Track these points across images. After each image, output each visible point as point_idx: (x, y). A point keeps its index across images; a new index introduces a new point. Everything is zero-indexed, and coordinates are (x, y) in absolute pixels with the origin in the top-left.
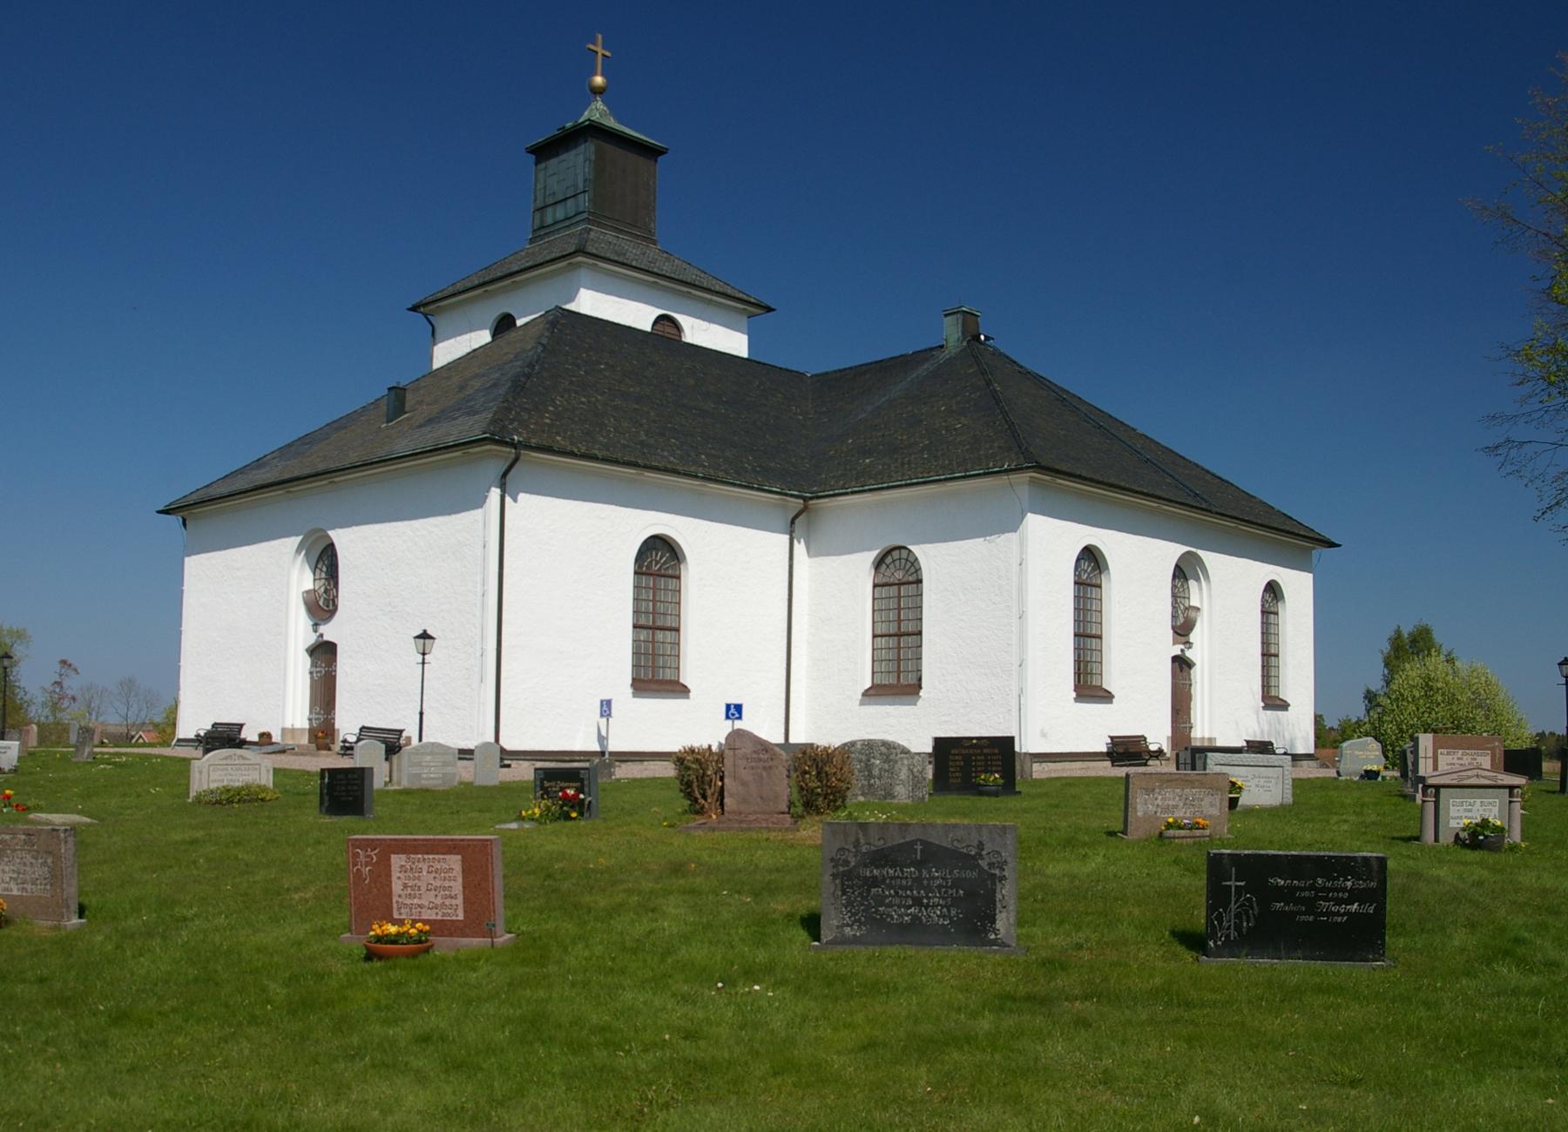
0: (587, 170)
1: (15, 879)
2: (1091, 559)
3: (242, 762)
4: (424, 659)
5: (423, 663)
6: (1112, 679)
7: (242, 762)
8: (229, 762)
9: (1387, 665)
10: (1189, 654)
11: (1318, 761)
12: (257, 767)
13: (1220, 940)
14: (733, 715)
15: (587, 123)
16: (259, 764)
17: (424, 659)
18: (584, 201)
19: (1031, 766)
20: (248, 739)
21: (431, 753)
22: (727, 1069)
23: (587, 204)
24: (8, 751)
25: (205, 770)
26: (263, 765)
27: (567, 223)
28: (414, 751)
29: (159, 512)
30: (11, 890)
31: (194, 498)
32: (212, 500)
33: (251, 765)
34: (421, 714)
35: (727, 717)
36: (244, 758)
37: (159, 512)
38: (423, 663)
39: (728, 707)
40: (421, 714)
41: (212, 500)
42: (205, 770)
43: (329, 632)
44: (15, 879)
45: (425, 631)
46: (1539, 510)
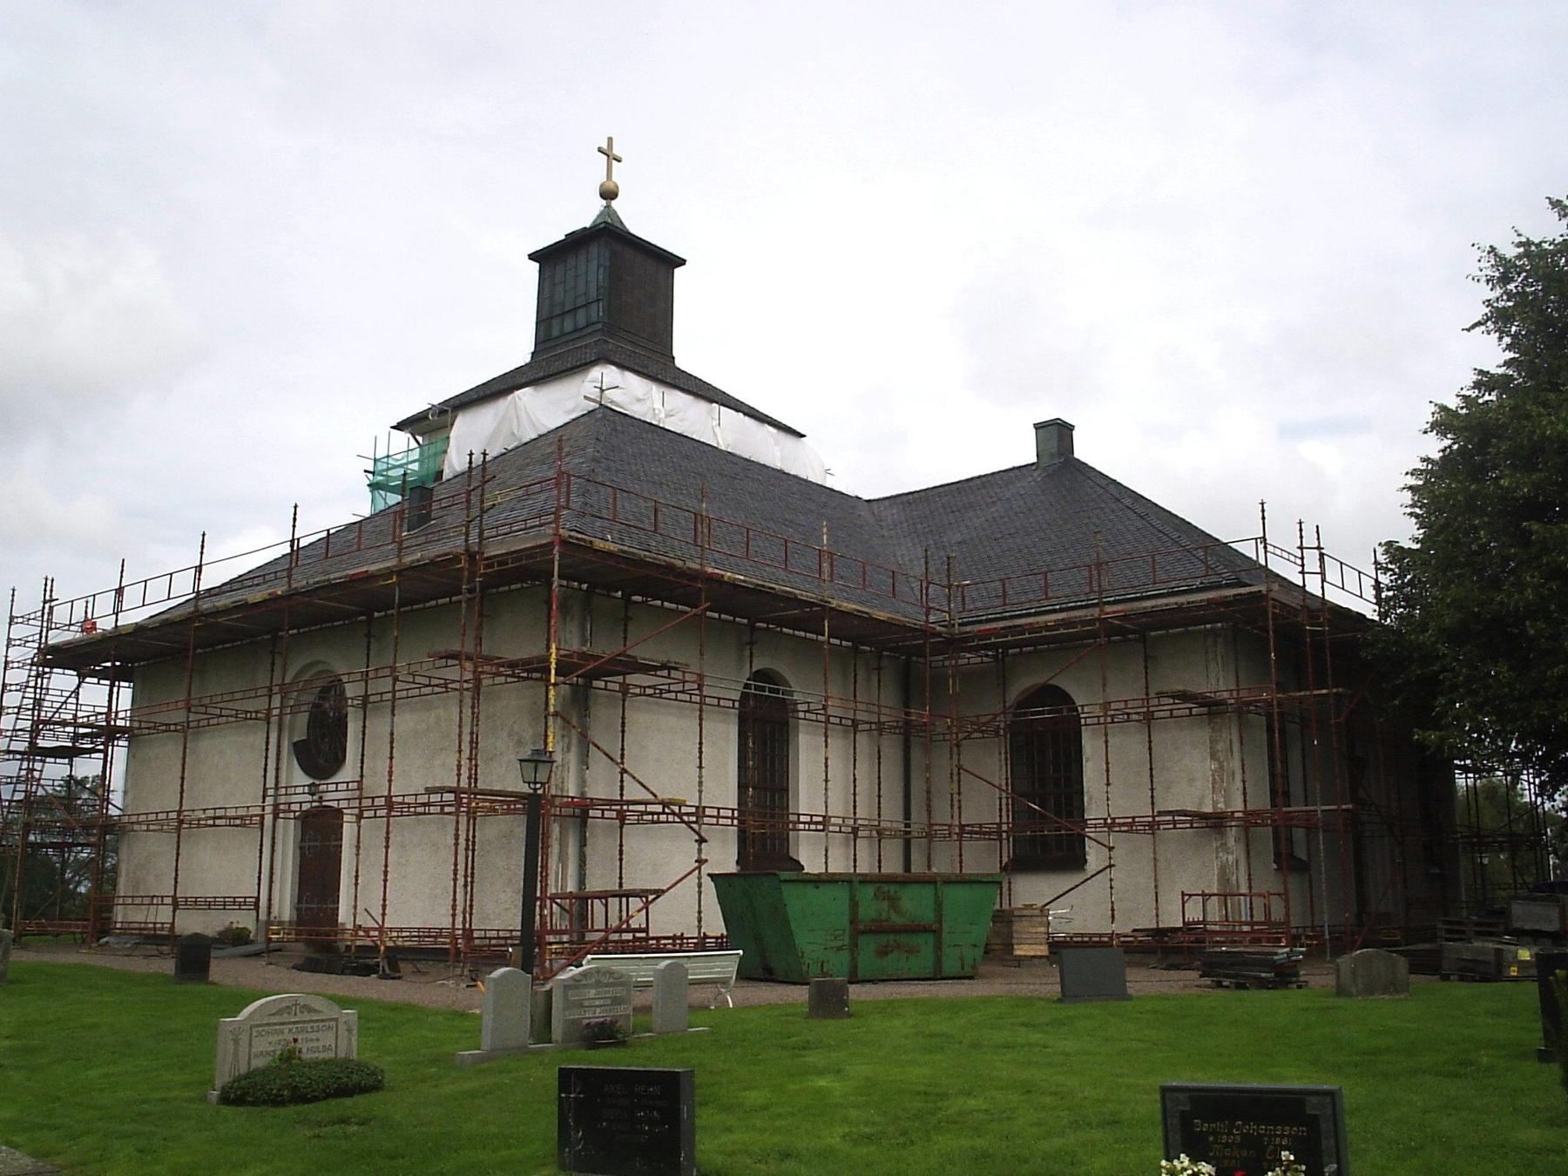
0: (601, 277)
3: (307, 1017)
7: (307, 1017)
8: (285, 1018)
9: (1558, 201)
10: (604, 203)
11: (223, 1075)
12: (333, 1023)
13: (1253, 628)
15: (602, 226)
16: (336, 1020)
18: (598, 311)
19: (1287, 915)
21: (598, 984)
23: (601, 314)
25: (244, 1037)
26: (341, 1020)
27: (577, 335)
28: (571, 982)
32: (980, 882)
33: (323, 1021)
36: (310, 1010)
41: (980, 882)
42: (244, 1037)
46: (1562, 236)
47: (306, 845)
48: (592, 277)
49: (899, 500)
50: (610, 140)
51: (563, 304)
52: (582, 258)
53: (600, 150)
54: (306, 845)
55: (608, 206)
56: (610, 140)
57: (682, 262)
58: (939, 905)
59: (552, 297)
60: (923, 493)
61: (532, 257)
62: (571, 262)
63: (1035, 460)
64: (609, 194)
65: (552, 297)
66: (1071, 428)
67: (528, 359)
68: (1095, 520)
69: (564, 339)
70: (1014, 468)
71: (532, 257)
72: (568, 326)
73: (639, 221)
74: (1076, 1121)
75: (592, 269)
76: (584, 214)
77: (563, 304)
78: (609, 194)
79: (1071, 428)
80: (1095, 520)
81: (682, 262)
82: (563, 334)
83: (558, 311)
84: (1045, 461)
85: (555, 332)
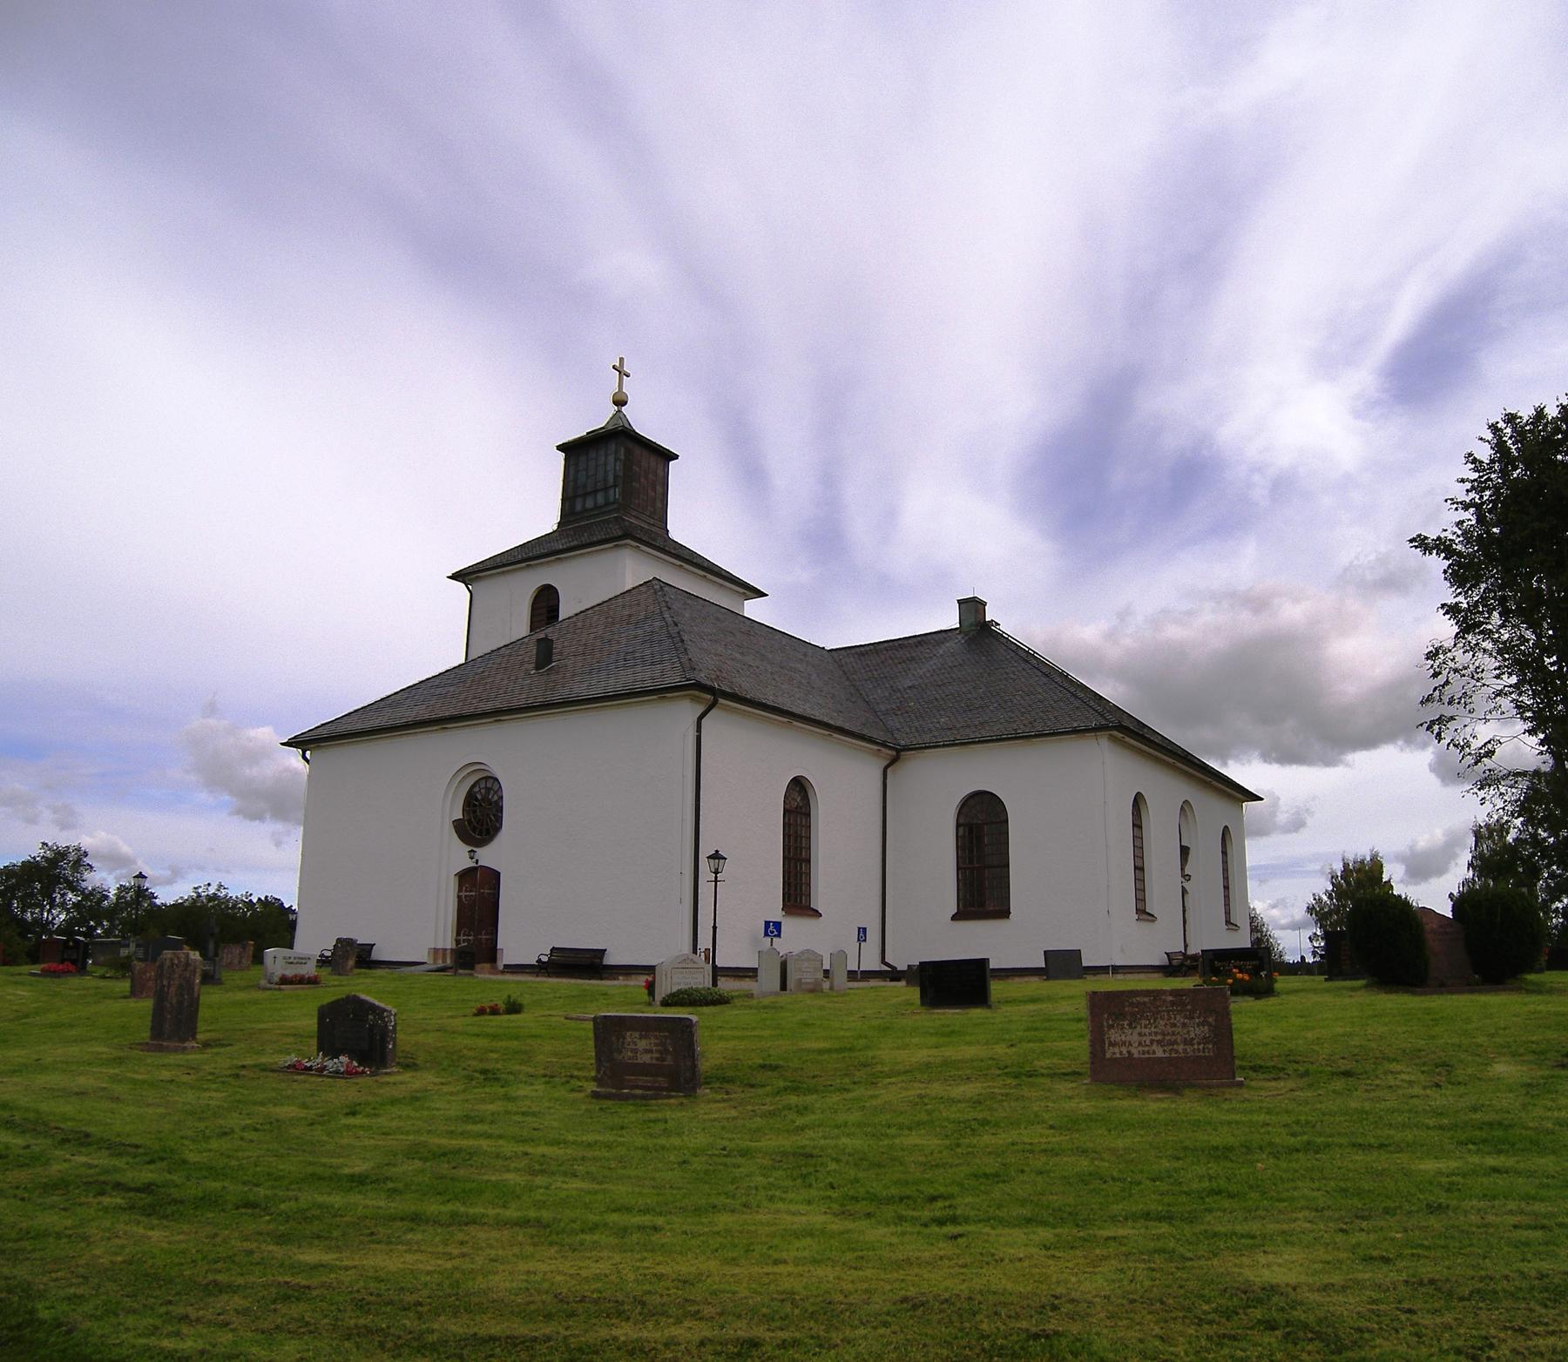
1: (1159, 1042)
2: (799, 788)
4: (716, 877)
5: (716, 881)
6: (818, 902)
14: (772, 932)
17: (716, 877)
20: (1289, 931)
22: (257, 1330)
24: (309, 962)
29: (282, 744)
30: (1154, 1052)
31: (324, 732)
34: (715, 928)
35: (766, 934)
37: (282, 744)
38: (716, 881)
39: (767, 924)
40: (715, 928)
43: (488, 856)
44: (1159, 1042)
45: (717, 851)
47: (463, 894)
48: (610, 467)
49: (853, 651)
50: (621, 360)
51: (585, 486)
52: (602, 452)
53: (614, 367)
54: (463, 894)
55: (619, 411)
56: (621, 360)
57: (675, 457)
58: (715, 984)
59: (575, 480)
60: (872, 647)
61: (560, 448)
62: (592, 454)
63: (958, 626)
64: (620, 402)
65: (575, 480)
66: (984, 604)
67: (555, 527)
68: (1012, 676)
69: (586, 515)
70: (941, 631)
71: (560, 448)
72: (590, 503)
73: (646, 422)
74: (528, 1289)
75: (610, 461)
76: (598, 417)
77: (585, 486)
78: (620, 402)
79: (984, 604)
80: (1012, 676)
81: (675, 457)
82: (585, 510)
83: (580, 492)
84: (965, 624)
85: (579, 507)
